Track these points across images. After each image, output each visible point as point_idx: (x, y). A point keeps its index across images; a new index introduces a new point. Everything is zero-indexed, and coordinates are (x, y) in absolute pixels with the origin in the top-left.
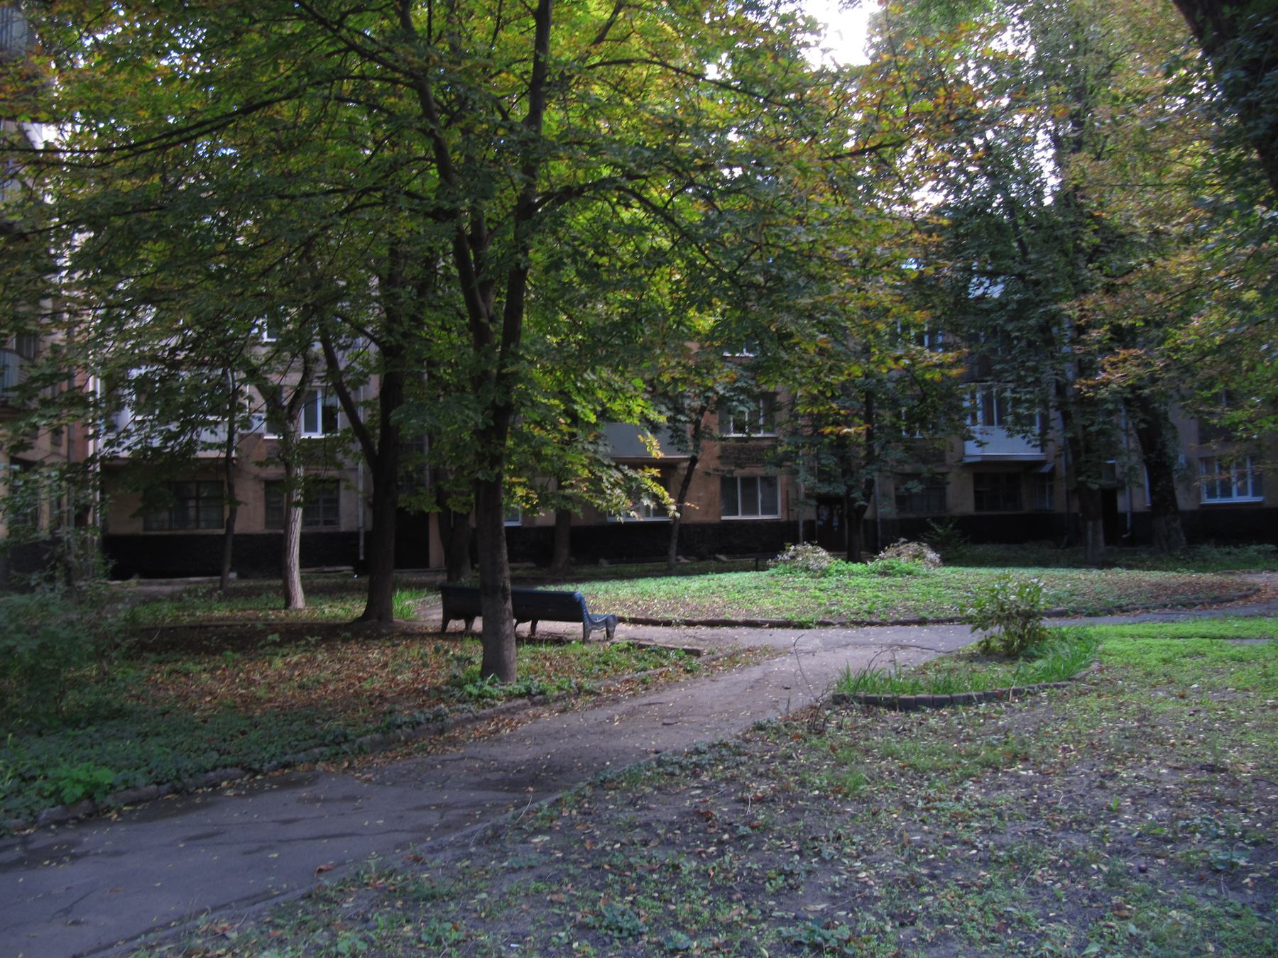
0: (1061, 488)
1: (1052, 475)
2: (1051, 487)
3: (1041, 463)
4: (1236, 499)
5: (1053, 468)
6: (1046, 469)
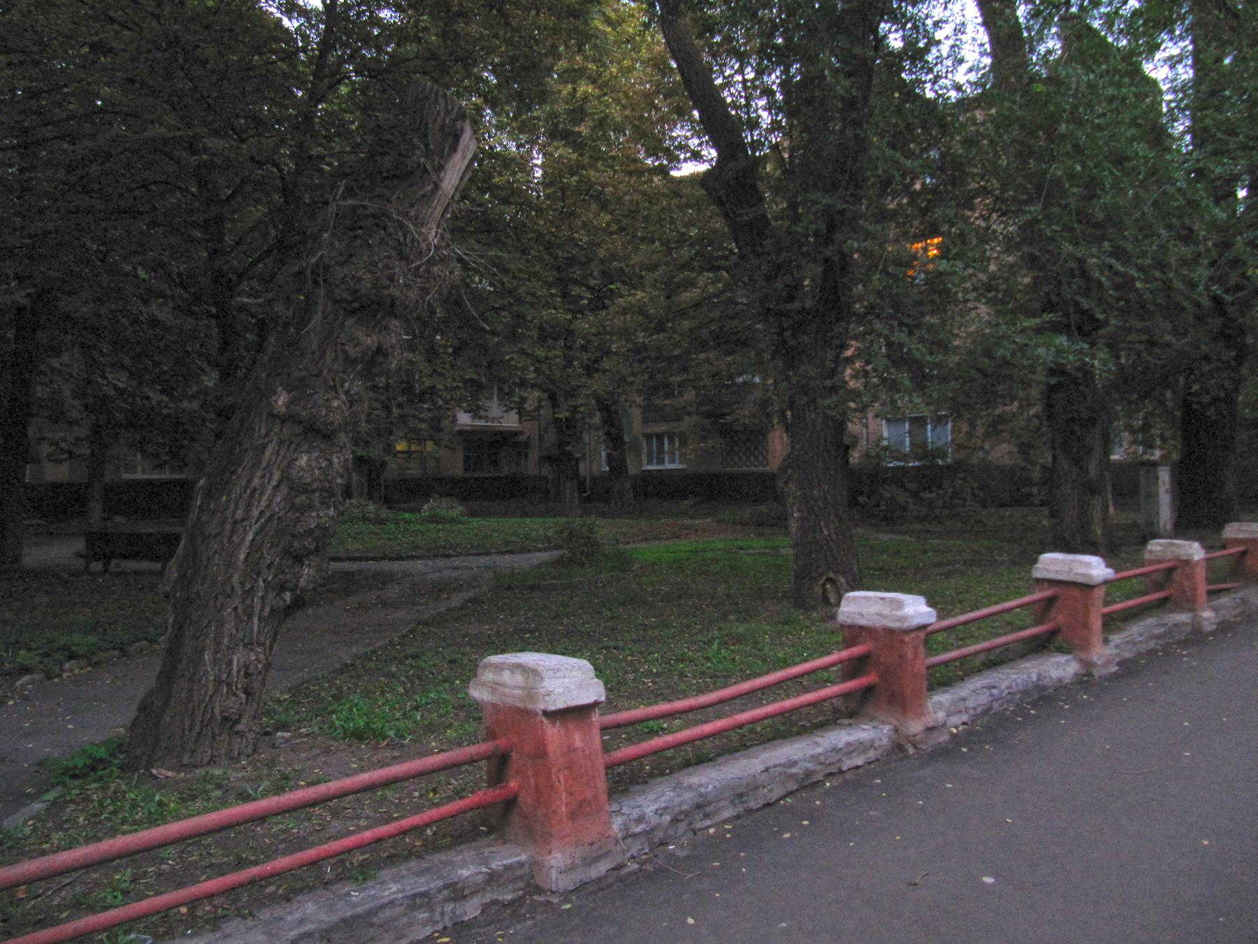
0: (534, 454)
1: (527, 444)
2: (526, 456)
3: (516, 434)
4: (668, 466)
5: (529, 438)
6: (522, 438)
